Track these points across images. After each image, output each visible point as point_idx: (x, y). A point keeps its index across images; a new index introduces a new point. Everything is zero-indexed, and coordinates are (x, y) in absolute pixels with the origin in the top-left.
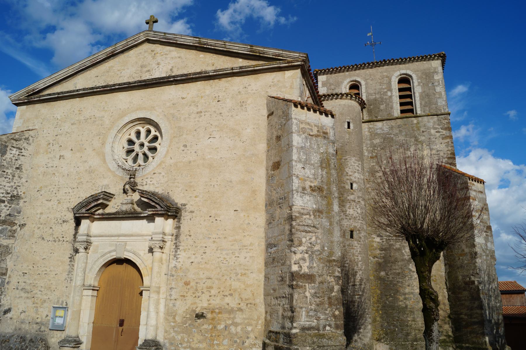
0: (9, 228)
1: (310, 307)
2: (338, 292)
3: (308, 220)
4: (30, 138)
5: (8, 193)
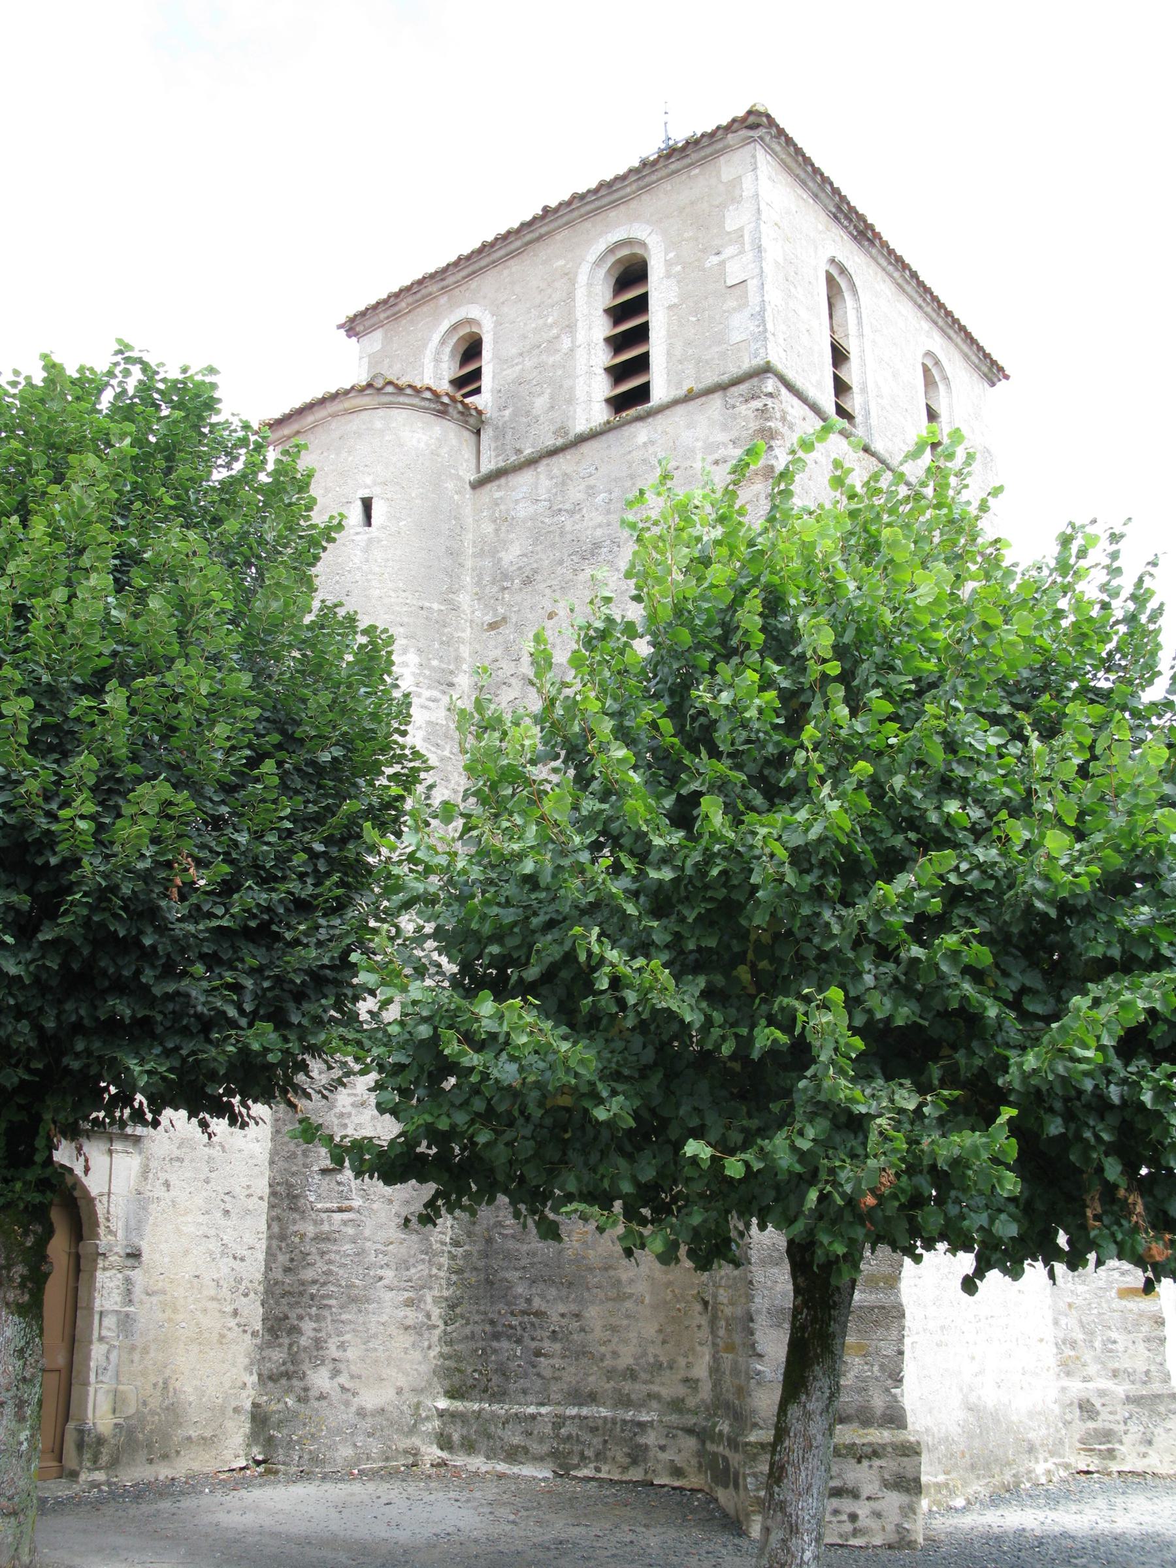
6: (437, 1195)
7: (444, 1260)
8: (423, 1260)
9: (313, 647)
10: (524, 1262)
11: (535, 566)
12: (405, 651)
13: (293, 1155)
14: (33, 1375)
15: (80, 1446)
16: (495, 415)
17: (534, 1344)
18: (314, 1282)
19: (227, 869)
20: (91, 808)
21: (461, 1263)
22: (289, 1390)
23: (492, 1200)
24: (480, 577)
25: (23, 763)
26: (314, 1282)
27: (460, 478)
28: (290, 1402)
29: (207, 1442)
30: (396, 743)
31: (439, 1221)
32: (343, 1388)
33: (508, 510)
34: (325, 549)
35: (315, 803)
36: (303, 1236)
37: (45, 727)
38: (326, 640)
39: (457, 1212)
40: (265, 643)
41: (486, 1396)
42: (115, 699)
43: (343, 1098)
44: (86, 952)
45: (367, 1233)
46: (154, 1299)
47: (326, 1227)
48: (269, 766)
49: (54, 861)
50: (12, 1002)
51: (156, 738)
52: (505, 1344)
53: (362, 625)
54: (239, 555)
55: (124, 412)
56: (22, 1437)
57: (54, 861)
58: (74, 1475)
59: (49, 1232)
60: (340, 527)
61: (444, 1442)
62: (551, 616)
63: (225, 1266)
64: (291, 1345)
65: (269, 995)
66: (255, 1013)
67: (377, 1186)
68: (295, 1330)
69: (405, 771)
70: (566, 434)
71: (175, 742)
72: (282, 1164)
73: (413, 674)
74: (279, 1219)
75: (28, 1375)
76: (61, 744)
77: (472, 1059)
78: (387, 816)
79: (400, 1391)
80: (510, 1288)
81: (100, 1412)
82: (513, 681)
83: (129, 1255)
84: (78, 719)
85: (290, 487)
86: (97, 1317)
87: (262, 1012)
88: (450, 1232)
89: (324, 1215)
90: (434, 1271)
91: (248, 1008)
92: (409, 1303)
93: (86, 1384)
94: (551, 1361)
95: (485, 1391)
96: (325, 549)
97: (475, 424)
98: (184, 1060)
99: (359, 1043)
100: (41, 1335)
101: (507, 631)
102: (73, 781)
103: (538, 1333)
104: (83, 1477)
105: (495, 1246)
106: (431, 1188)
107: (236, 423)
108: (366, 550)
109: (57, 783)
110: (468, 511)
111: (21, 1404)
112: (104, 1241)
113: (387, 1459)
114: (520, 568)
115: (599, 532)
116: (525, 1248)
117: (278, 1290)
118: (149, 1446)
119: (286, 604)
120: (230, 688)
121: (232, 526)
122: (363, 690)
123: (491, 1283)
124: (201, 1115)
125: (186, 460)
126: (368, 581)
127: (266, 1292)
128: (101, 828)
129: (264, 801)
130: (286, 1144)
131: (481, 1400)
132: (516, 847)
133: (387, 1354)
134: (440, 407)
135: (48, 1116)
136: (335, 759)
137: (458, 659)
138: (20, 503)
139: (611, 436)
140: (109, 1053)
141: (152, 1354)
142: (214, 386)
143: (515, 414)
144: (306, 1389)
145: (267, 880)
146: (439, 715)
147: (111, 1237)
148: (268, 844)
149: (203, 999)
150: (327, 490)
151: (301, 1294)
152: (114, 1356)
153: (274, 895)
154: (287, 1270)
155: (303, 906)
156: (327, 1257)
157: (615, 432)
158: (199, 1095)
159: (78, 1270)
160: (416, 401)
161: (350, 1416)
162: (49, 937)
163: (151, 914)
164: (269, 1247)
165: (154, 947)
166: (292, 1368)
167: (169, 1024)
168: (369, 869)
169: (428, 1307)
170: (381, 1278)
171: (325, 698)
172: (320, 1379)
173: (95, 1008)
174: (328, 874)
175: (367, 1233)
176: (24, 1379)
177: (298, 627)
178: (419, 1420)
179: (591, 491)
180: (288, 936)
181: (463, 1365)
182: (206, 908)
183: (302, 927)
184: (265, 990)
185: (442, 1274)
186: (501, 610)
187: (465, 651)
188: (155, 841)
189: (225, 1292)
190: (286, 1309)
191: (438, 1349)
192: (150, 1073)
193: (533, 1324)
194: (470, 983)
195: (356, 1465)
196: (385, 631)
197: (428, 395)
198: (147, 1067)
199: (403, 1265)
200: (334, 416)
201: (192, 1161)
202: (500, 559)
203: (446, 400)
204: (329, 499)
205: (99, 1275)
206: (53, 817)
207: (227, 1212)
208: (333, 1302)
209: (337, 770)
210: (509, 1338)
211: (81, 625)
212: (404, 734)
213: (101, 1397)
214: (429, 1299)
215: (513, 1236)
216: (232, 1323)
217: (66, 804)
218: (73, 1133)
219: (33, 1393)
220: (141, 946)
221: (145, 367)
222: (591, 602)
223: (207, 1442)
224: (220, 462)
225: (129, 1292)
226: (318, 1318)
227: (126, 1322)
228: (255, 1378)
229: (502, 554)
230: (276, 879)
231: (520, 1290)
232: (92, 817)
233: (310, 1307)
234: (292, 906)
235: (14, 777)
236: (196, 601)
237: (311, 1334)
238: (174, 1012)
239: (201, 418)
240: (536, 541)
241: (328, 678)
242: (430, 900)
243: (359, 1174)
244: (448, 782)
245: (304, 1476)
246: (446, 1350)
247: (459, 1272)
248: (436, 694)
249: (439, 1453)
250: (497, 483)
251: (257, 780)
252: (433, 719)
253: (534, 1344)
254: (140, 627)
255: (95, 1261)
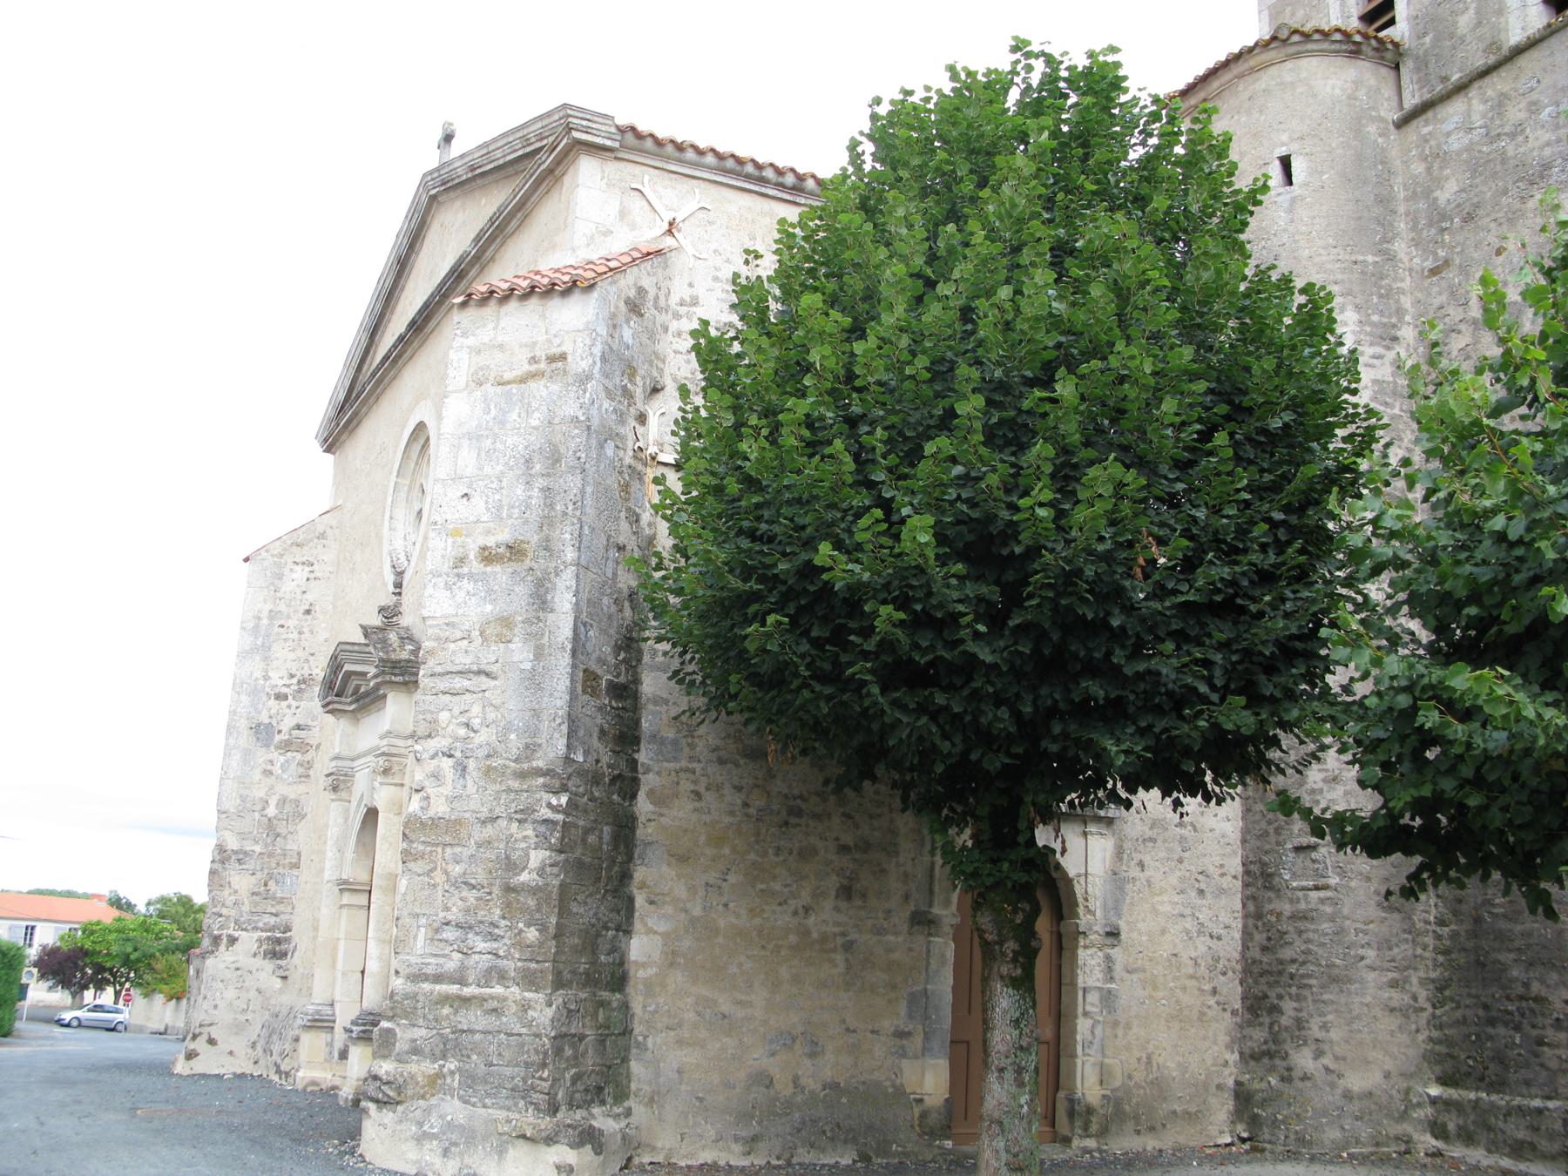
0: (298, 756)
1: (442, 915)
2: (541, 871)
3: (461, 655)
4: (329, 531)
5: (292, 676)
6: (1421, 868)
7: (1429, 940)
8: (1406, 940)
9: (1252, 314)
10: (1517, 944)
11: (1476, 200)
12: (1342, 310)
13: (1266, 834)
14: (1029, 1044)
15: (1071, 1114)
16: (1414, 45)
17: (1535, 1032)
18: (1293, 961)
19: (1185, 542)
20: (1047, 495)
21: (1448, 943)
22: (1272, 1069)
23: (1486, 877)
24: (1415, 222)
25: (981, 459)
26: (1293, 961)
27: (1382, 120)
28: (1273, 1082)
29: (1191, 1117)
30: (1346, 401)
31: (1423, 897)
32: (1327, 1069)
33: (1439, 145)
34: (1252, 213)
35: (1269, 471)
36: (1279, 915)
37: (1001, 422)
38: (1265, 304)
39: (1443, 887)
40: (1201, 315)
41: (1483, 1085)
42: (1065, 388)
43: (1314, 775)
44: (1055, 636)
45: (1346, 911)
46: (1135, 977)
47: (1303, 906)
48: (1221, 438)
49: (1018, 550)
50: (991, 690)
51: (1106, 422)
52: (1501, 1030)
53: (1299, 283)
54: (1166, 231)
55: (1034, 107)
56: (1023, 1101)
57: (1018, 550)
58: (1066, 1141)
59: (1036, 912)
60: (1265, 188)
61: (1438, 1131)
62: (1499, 252)
63: (1202, 945)
64: (1271, 1025)
65: (1240, 668)
66: (1226, 687)
67: (1360, 862)
68: (1275, 1010)
69: (1361, 431)
70: (1499, 49)
71: (1125, 424)
72: (1254, 843)
73: (1353, 332)
74: (1254, 898)
75: (1024, 1044)
76: (1016, 437)
77: (1458, 730)
78: (1344, 480)
79: (1387, 1075)
80: (1505, 970)
81: (1088, 1084)
82: (1463, 327)
83: (1109, 934)
84: (1030, 412)
85: (1208, 155)
86: (1080, 993)
87: (1232, 686)
88: (1434, 911)
89: (1300, 894)
90: (1419, 951)
91: (1219, 682)
92: (1394, 984)
93: (1074, 1056)
94: (1557, 1052)
95: (1482, 1079)
96: (1252, 213)
97: (1393, 58)
98: (1158, 737)
99: (1333, 719)
100: (1034, 1007)
101: (1452, 275)
102: (1031, 471)
103: (1539, 1020)
104: (1076, 1143)
105: (1485, 926)
106: (1417, 859)
107: (1145, 100)
108: (1290, 210)
109: (1015, 476)
110: (1394, 153)
111: (1019, 1071)
112: (1084, 920)
113: (1377, 1145)
114: (1459, 205)
115: (1547, 152)
116: (1519, 928)
117: (1256, 969)
118: (1136, 1118)
119: (1218, 272)
120: (1174, 363)
121: (1159, 203)
122: (1307, 351)
123: (1483, 965)
124: (1175, 794)
125: (1101, 145)
126: (1296, 242)
127: (1244, 971)
128: (1060, 514)
129: (1218, 474)
130: (1258, 822)
131: (1477, 1089)
132: (1487, 503)
133: (1370, 1040)
134: (1352, 48)
135: (1028, 799)
136: (1286, 426)
137: (1400, 312)
138: (950, 211)
139: (1554, 41)
140: (1086, 736)
141: (1135, 1030)
142: (1118, 65)
143: (1436, 40)
144: (1289, 1069)
145: (1230, 553)
146: (1385, 371)
147: (1092, 910)
148: (1227, 517)
149: (1173, 676)
150: (1242, 154)
151: (1280, 973)
152: (1098, 1031)
153: (1237, 569)
154: (1264, 949)
155: (1266, 578)
156: (1305, 936)
157: (1558, 35)
158: (1174, 773)
159: (1060, 948)
160: (1325, 46)
161: (1336, 1097)
162: (1017, 622)
163: (1116, 595)
164: (1245, 927)
165: (1122, 628)
166: (1273, 1047)
167: (1140, 704)
168: (1329, 537)
169: (1414, 989)
170: (1362, 958)
171: (1269, 363)
172: (1303, 1060)
173: (1069, 691)
174: (1289, 543)
175: (1346, 911)
176: (1021, 1048)
177: (1233, 293)
178: (1410, 1106)
179: (1534, 108)
180: (1253, 608)
181: (1456, 1051)
182: (1170, 585)
183: (1267, 598)
184: (1234, 664)
185: (1427, 954)
186: (1442, 253)
187: (1406, 302)
188: (1112, 523)
189: (1203, 970)
190: (1265, 988)
191: (1427, 1033)
192: (1126, 752)
193: (1532, 1011)
194: (1448, 652)
195: (1344, 1148)
196: (1323, 288)
197: (1338, 37)
198: (1124, 747)
199: (1385, 945)
200: (1241, 76)
201: (1165, 841)
202: (1436, 199)
203: (1358, 38)
204: (1250, 162)
205: (1080, 952)
206: (1014, 508)
207: (1201, 892)
208: (1313, 982)
209: (1289, 436)
210: (1506, 1024)
211: (1029, 320)
212: (1354, 392)
213: (1088, 1068)
214: (1415, 981)
215: (1505, 916)
216: (1212, 1001)
217: (1026, 493)
218: (1049, 816)
219: (1030, 1061)
220: (1111, 628)
221: (1049, 60)
222: (1543, 229)
223: (1191, 1117)
224: (1133, 141)
225: (1110, 969)
226: (1298, 998)
227: (1108, 998)
228: (1236, 1056)
229: (1438, 193)
230: (1237, 551)
231: (1515, 973)
232: (1050, 504)
233: (1290, 986)
234: (1256, 578)
235: (973, 474)
236: (1133, 283)
237: (1292, 1013)
238: (1145, 692)
239: (1110, 99)
240: (1474, 173)
241: (1271, 343)
242: (1399, 564)
243: (1340, 847)
244: (1403, 443)
245: (1291, 1156)
246: (1435, 1034)
247: (1446, 952)
248: (1379, 350)
249: (1434, 1142)
250: (1424, 117)
251: (1210, 453)
252: (1379, 377)
253: (1535, 1032)
254: (1081, 316)
255: (1076, 939)
